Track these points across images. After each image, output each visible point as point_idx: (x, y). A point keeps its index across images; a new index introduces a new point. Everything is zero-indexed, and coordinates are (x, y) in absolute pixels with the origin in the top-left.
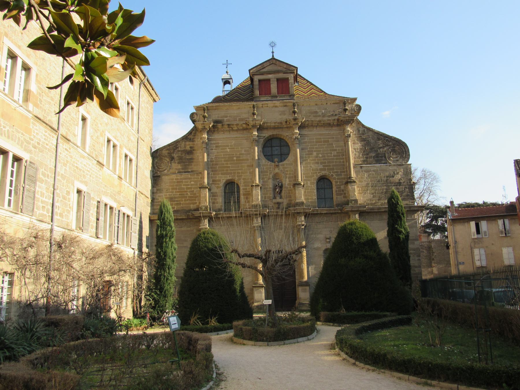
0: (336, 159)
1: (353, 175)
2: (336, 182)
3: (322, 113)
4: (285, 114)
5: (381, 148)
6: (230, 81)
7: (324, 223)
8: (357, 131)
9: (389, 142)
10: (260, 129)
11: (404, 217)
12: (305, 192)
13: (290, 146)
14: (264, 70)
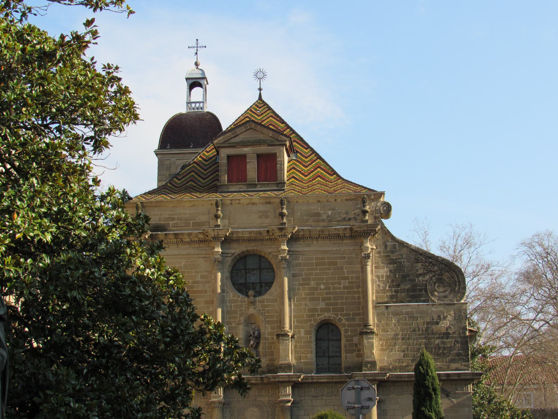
0: (348, 293)
1: (372, 319)
2: (347, 331)
3: (328, 216)
4: (267, 217)
5: (421, 275)
7: (324, 398)
8: (383, 247)
9: (434, 265)
10: (227, 241)
11: (435, 394)
12: (296, 346)
13: (275, 270)
14: (237, 139)
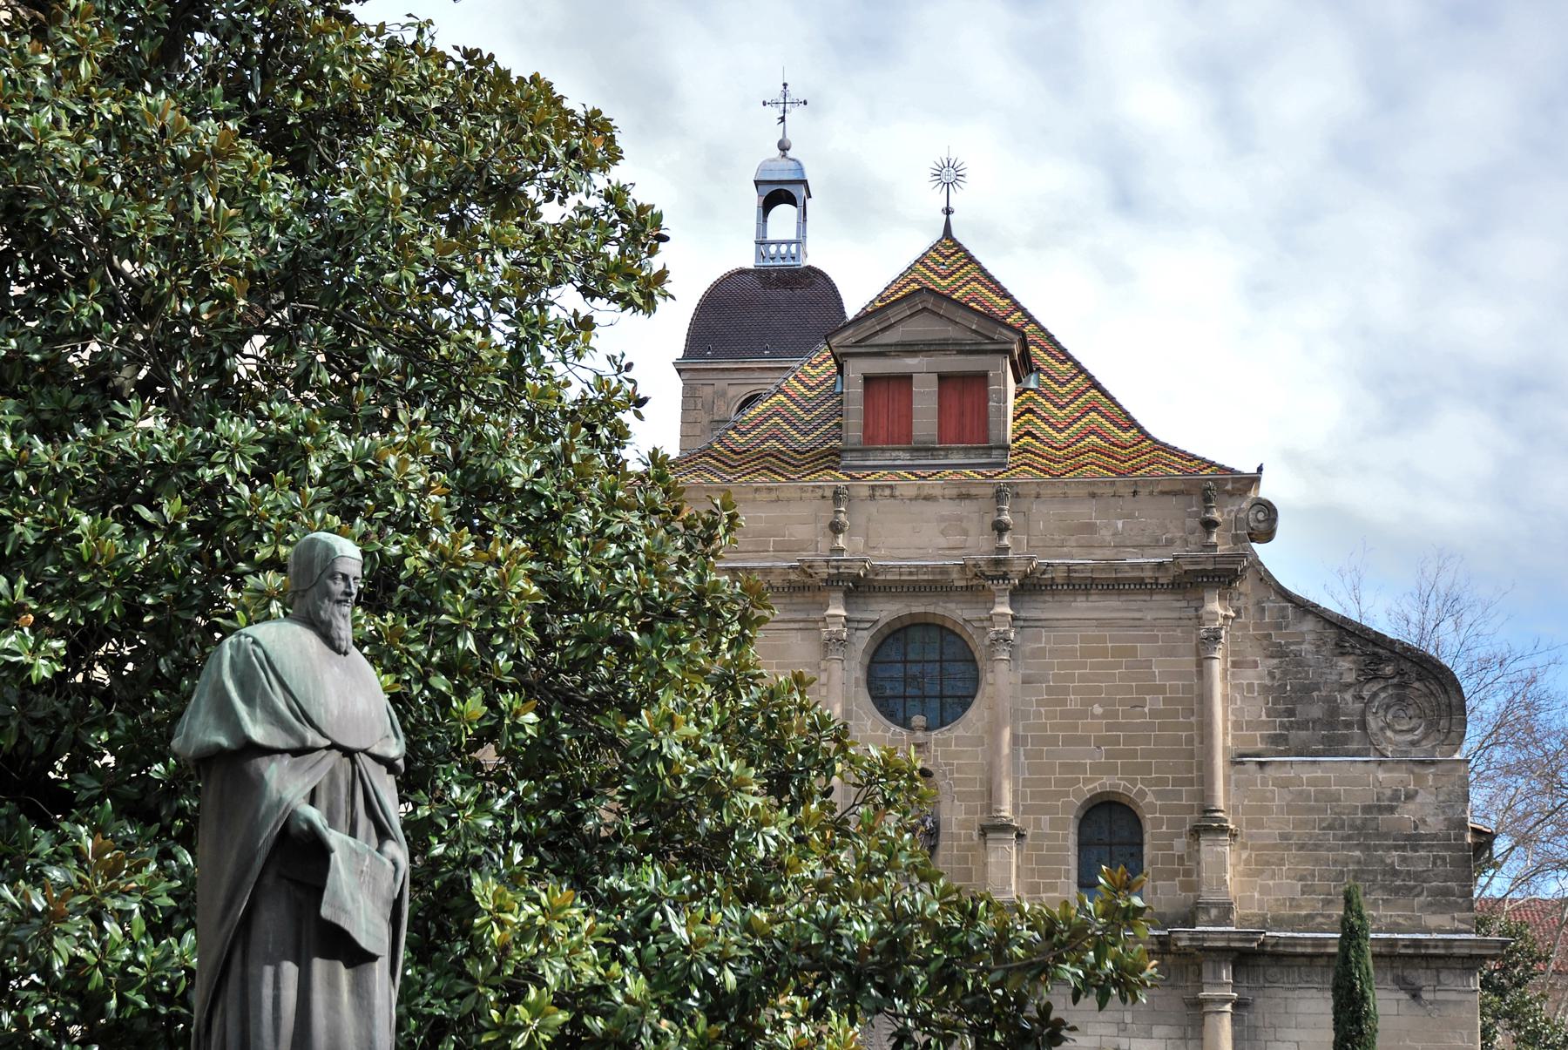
0: (1162, 727)
6: (798, 192)
